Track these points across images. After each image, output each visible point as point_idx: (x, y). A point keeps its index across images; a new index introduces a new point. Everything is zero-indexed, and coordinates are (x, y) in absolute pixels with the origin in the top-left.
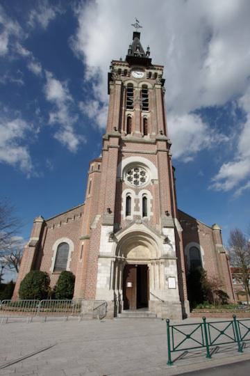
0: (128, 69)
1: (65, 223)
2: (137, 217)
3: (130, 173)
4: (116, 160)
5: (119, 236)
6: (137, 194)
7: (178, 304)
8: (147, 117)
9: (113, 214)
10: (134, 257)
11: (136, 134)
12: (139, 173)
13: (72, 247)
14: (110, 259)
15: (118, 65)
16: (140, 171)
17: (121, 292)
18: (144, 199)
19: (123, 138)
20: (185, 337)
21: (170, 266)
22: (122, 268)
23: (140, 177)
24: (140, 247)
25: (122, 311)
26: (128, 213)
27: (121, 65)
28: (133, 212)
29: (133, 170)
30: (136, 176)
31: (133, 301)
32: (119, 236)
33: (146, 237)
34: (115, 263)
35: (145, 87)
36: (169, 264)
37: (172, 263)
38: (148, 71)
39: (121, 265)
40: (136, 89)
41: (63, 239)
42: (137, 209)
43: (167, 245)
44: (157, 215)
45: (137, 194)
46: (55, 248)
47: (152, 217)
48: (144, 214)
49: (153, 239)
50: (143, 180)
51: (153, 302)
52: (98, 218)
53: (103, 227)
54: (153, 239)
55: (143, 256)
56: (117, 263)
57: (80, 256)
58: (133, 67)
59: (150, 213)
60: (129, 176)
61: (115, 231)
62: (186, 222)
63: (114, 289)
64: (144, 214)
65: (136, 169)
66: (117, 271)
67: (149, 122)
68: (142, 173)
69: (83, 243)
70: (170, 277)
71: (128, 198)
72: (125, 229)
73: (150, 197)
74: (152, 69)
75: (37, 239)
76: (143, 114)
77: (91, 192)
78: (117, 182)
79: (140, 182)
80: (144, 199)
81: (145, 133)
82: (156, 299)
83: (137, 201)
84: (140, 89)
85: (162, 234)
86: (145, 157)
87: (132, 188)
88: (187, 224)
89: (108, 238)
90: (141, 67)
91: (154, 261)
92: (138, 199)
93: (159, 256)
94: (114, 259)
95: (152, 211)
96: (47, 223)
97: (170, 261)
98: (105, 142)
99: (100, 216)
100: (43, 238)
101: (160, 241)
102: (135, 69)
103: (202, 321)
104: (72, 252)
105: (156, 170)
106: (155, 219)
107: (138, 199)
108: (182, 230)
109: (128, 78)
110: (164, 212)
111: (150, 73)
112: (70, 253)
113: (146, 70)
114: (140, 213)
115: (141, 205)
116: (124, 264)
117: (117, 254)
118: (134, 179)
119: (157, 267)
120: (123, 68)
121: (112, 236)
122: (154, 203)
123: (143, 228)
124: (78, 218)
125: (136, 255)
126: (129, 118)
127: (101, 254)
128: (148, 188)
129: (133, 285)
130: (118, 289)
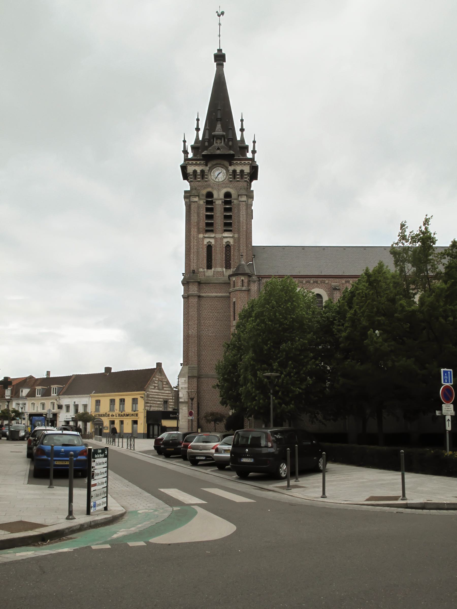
0: (206, 169)
120: (198, 169)
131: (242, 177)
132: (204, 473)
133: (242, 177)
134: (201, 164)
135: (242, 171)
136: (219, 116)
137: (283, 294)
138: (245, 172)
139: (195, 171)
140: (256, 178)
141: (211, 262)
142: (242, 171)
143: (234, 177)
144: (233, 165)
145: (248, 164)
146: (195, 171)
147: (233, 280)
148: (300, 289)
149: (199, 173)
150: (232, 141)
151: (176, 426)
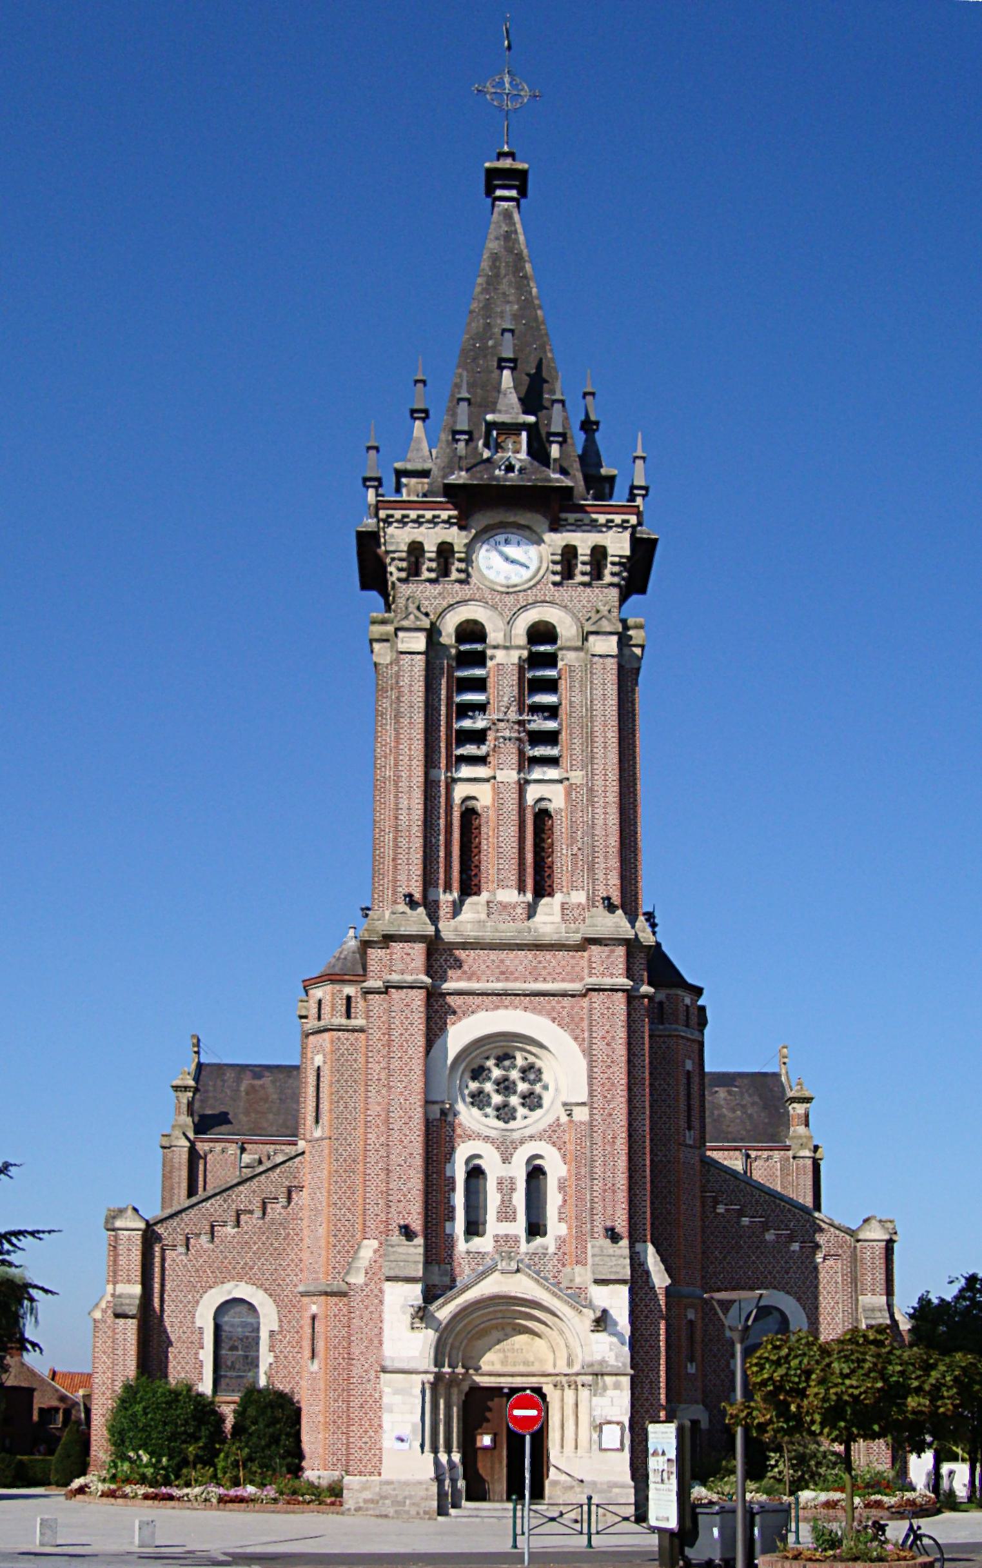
0: (457, 538)
1: (230, 1230)
2: (505, 1242)
3: (479, 1073)
4: (420, 1041)
5: (444, 1312)
6: (506, 1160)
7: (623, 1486)
8: (551, 807)
9: (420, 1241)
10: (498, 1368)
11: (504, 906)
12: (515, 1075)
13: (269, 1319)
14: (418, 1379)
15: (403, 522)
16: (520, 1062)
17: (456, 1457)
18: (535, 1174)
19: (449, 930)
20: (546, 1520)
21: (610, 1393)
22: (457, 1398)
23: (522, 1087)
24: (521, 1340)
25: (464, 1503)
26: (474, 1228)
27: (418, 521)
28: (493, 1226)
29: (490, 1063)
30: (504, 1086)
31: (498, 1477)
32: (444, 1312)
33: (536, 1313)
34: (434, 1386)
35: (542, 633)
36: (605, 1388)
37: (617, 1386)
38: (556, 540)
39: (455, 1391)
40: (500, 655)
41: (229, 1286)
42: (506, 1215)
43: (603, 1337)
44: (580, 1238)
45: (506, 1160)
46: (205, 1319)
47: (561, 1242)
48: (535, 1229)
49: (554, 1314)
50: (532, 1101)
51: (555, 1483)
52: (368, 1250)
53: (388, 1286)
54: (554, 1314)
55: (526, 1363)
56: (439, 1386)
57: (307, 1353)
58: (482, 519)
59: (556, 1227)
60: (474, 1086)
61: (431, 1295)
62: (741, 1213)
63: (435, 1450)
64: (535, 1229)
65: (504, 1058)
66: (442, 1406)
67: (560, 828)
68: (531, 1072)
69: (314, 1309)
70: (609, 1423)
71: (475, 1174)
72: (467, 1288)
73: (556, 1169)
74: (578, 526)
75: (137, 1289)
76: (533, 793)
77: (325, 1118)
78: (428, 1123)
79: (521, 1111)
80: (535, 1174)
81: (542, 889)
82: (564, 1477)
83: (506, 1186)
84: (514, 656)
85: (590, 1306)
86: (534, 1010)
87: (487, 1138)
88: (745, 1221)
89: (407, 1319)
90: (523, 518)
91: (564, 1379)
92: (512, 1180)
93: (576, 1368)
94: (431, 1378)
95: (560, 1220)
96: (159, 1229)
97: (608, 1380)
98: (370, 951)
99: (375, 1244)
100: (157, 1286)
101: (580, 1323)
102: (484, 535)
103: (586, 1501)
104: (272, 1333)
105: (581, 1064)
106: (570, 1248)
107: (512, 1180)
108: (668, 1281)
109: (460, 591)
110: (599, 1229)
111: (569, 553)
112: (264, 1335)
113: (549, 537)
114: (519, 1227)
115: (519, 1199)
116: (466, 1387)
117: (438, 1363)
118: (497, 1099)
119: (569, 1394)
120: (431, 538)
121: (422, 1315)
122: (571, 1191)
123: (522, 1286)
124: (276, 1210)
125: (504, 1363)
126: (470, 815)
127: (388, 1364)
128: (552, 1134)
129: (494, 1440)
130: (449, 1451)
131: (597, 573)
132: (67, 1558)
133: (597, 573)
134: (439, 520)
135: (599, 553)
136: (508, 354)
137: (140, 1420)
138: (610, 551)
139: (416, 549)
140: (642, 590)
141: (451, 835)
142: (599, 553)
143: (568, 573)
144: (564, 526)
145: (623, 526)
146: (416, 549)
147: (316, 1065)
148: (146, 1470)
149: (432, 552)
150: (561, 444)
151: (621, 951)
